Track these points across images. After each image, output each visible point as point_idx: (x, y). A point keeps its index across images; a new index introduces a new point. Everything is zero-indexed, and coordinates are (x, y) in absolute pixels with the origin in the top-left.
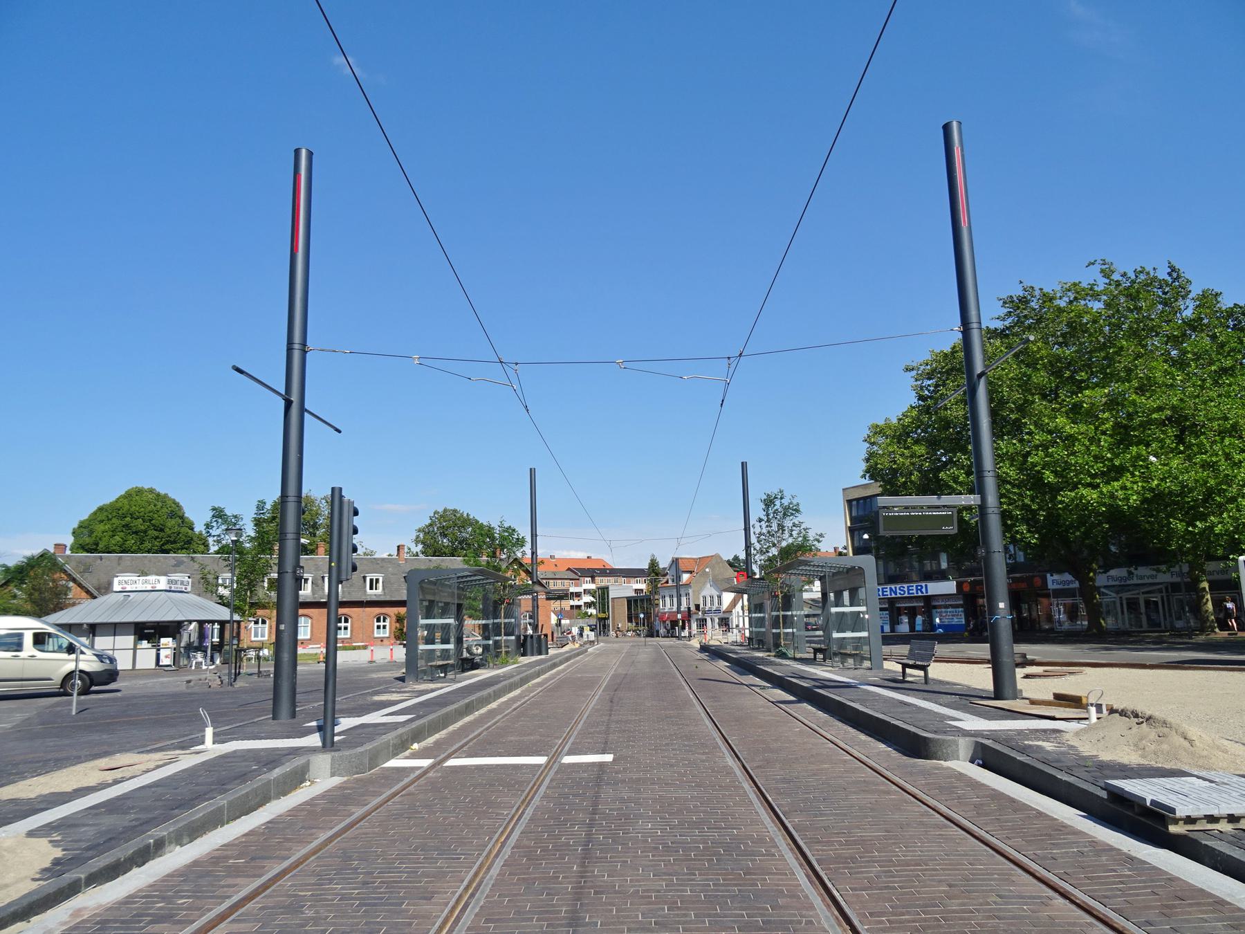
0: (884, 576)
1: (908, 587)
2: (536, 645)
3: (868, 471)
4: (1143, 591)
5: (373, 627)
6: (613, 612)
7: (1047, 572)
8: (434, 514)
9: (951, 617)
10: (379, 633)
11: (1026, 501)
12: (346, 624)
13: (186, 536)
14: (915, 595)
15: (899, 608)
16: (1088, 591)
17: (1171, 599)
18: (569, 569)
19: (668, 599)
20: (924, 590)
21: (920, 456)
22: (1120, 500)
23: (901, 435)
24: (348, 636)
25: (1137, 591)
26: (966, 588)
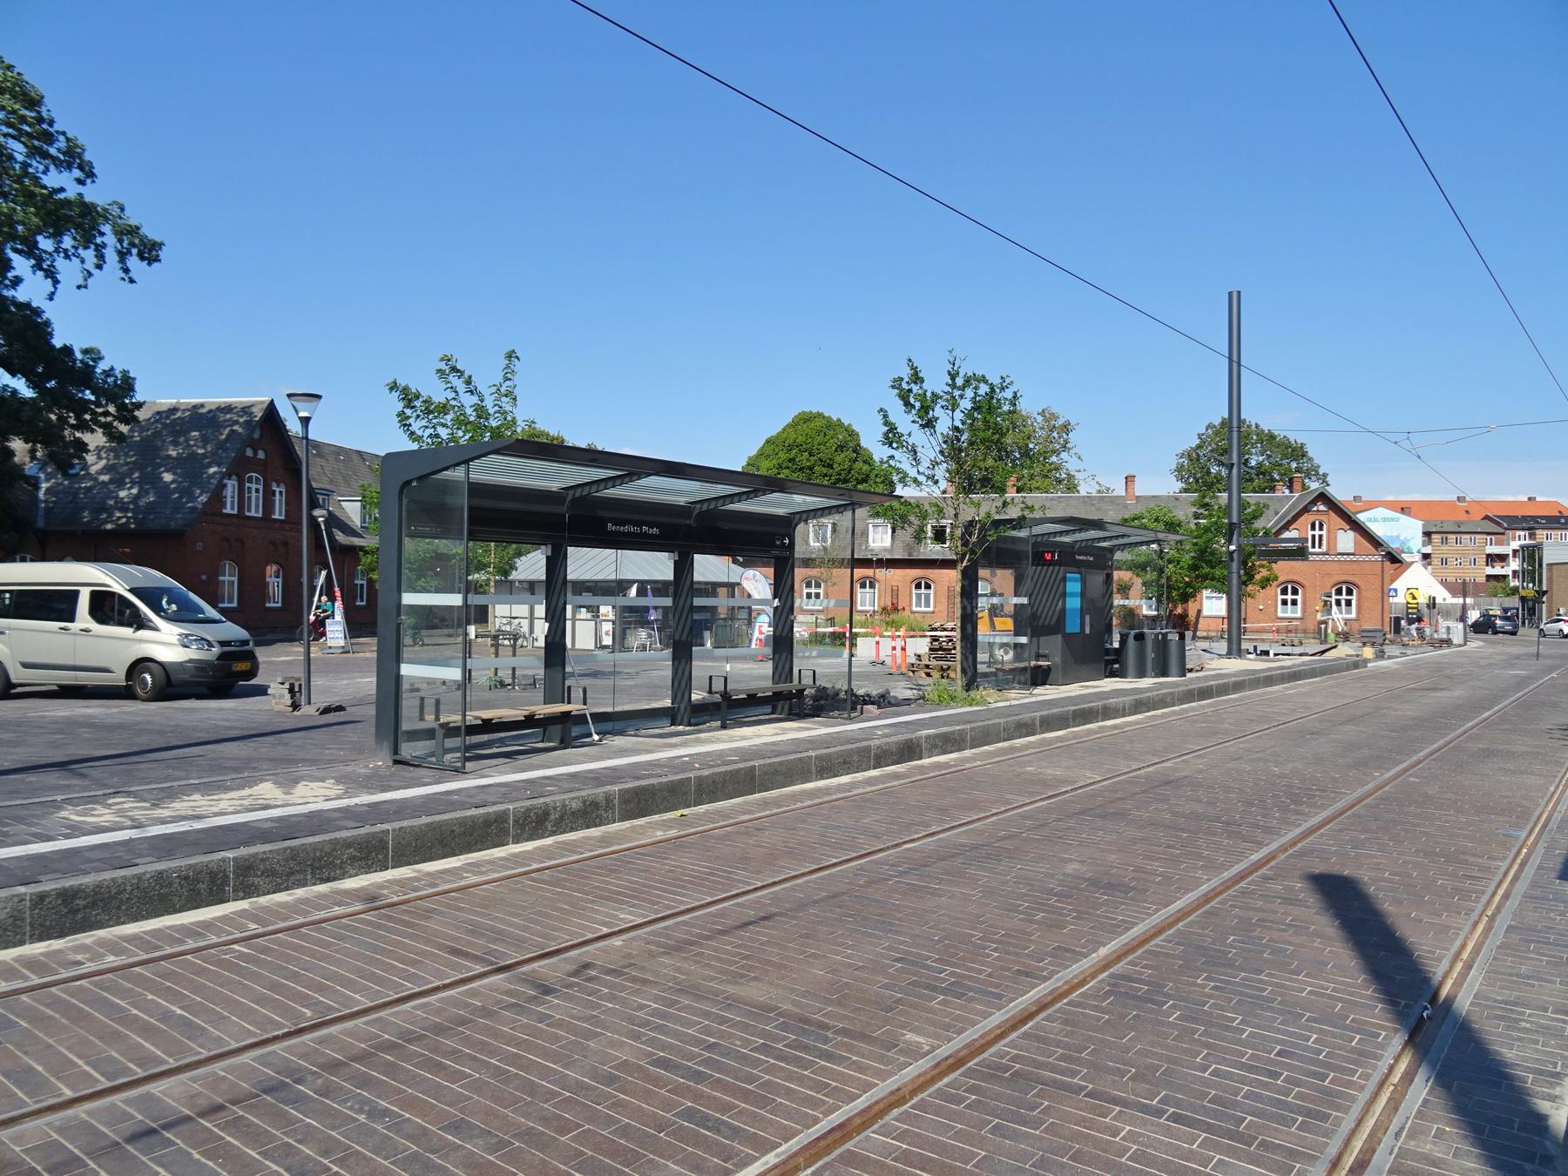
2: (1151, 655)
5: (1277, 601)
12: (1294, 597)
13: (859, 474)
18: (1487, 518)
24: (1353, 615)
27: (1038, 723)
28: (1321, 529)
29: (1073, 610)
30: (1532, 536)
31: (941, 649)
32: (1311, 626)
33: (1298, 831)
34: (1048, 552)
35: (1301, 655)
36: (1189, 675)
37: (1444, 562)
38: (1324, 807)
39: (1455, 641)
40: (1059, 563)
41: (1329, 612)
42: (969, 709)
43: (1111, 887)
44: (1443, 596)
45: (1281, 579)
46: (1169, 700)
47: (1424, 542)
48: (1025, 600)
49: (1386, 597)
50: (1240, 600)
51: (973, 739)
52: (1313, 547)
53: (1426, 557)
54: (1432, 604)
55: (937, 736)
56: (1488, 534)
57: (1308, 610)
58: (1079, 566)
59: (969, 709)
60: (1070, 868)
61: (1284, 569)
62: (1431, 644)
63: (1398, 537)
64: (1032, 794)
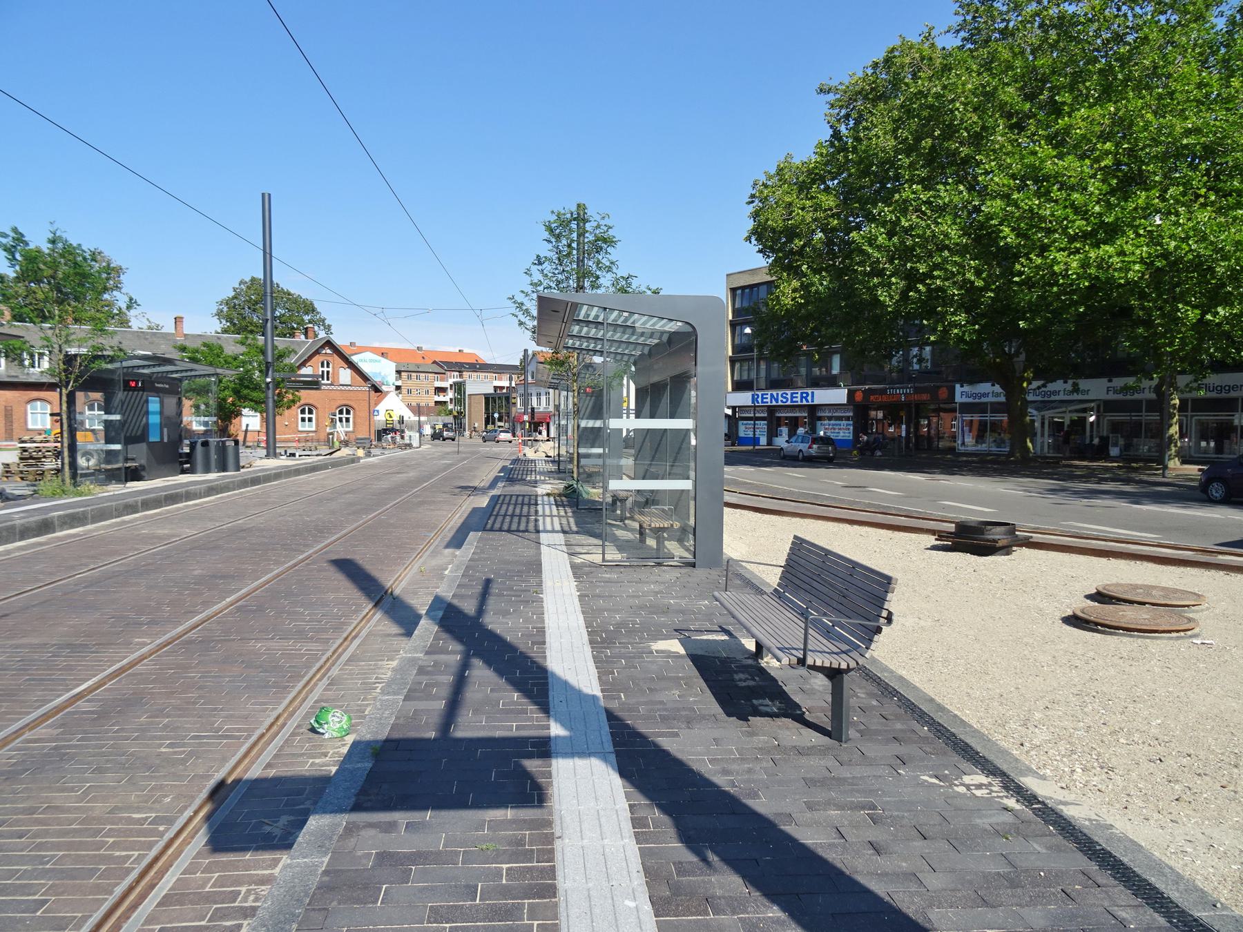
0: (766, 381)
1: (792, 394)
2: (214, 457)
3: (754, 232)
4: (1069, 409)
5: (297, 419)
6: (470, 411)
7: (958, 381)
8: (240, 285)
9: (837, 431)
10: (303, 426)
11: (968, 275)
12: (310, 416)
14: (799, 403)
15: (780, 417)
16: (1014, 405)
17: (1101, 419)
18: (435, 362)
19: (543, 398)
20: (809, 398)
21: (826, 210)
22: (1115, 270)
23: (809, 180)
24: (351, 429)
25: (1064, 409)
26: (859, 397)
27: (140, 504)
28: (328, 367)
29: (154, 424)
30: (461, 376)
31: (31, 458)
32: (323, 436)
33: (323, 544)
34: (133, 381)
35: (317, 455)
36: (242, 470)
37: (409, 391)
38: (335, 533)
39: (414, 446)
40: (143, 389)
41: (335, 427)
42: (79, 499)
43: (223, 577)
44: (409, 416)
45: (302, 402)
46: (231, 486)
47: (396, 377)
48: (117, 417)
49: (372, 416)
50: (274, 416)
51: (93, 517)
52: (323, 379)
53: (398, 388)
54: (401, 421)
55: (67, 516)
56: (436, 373)
57: (321, 425)
58: (158, 392)
59: (79, 499)
60: (196, 573)
61: (306, 396)
62: (400, 447)
63: (380, 373)
64: (154, 544)
